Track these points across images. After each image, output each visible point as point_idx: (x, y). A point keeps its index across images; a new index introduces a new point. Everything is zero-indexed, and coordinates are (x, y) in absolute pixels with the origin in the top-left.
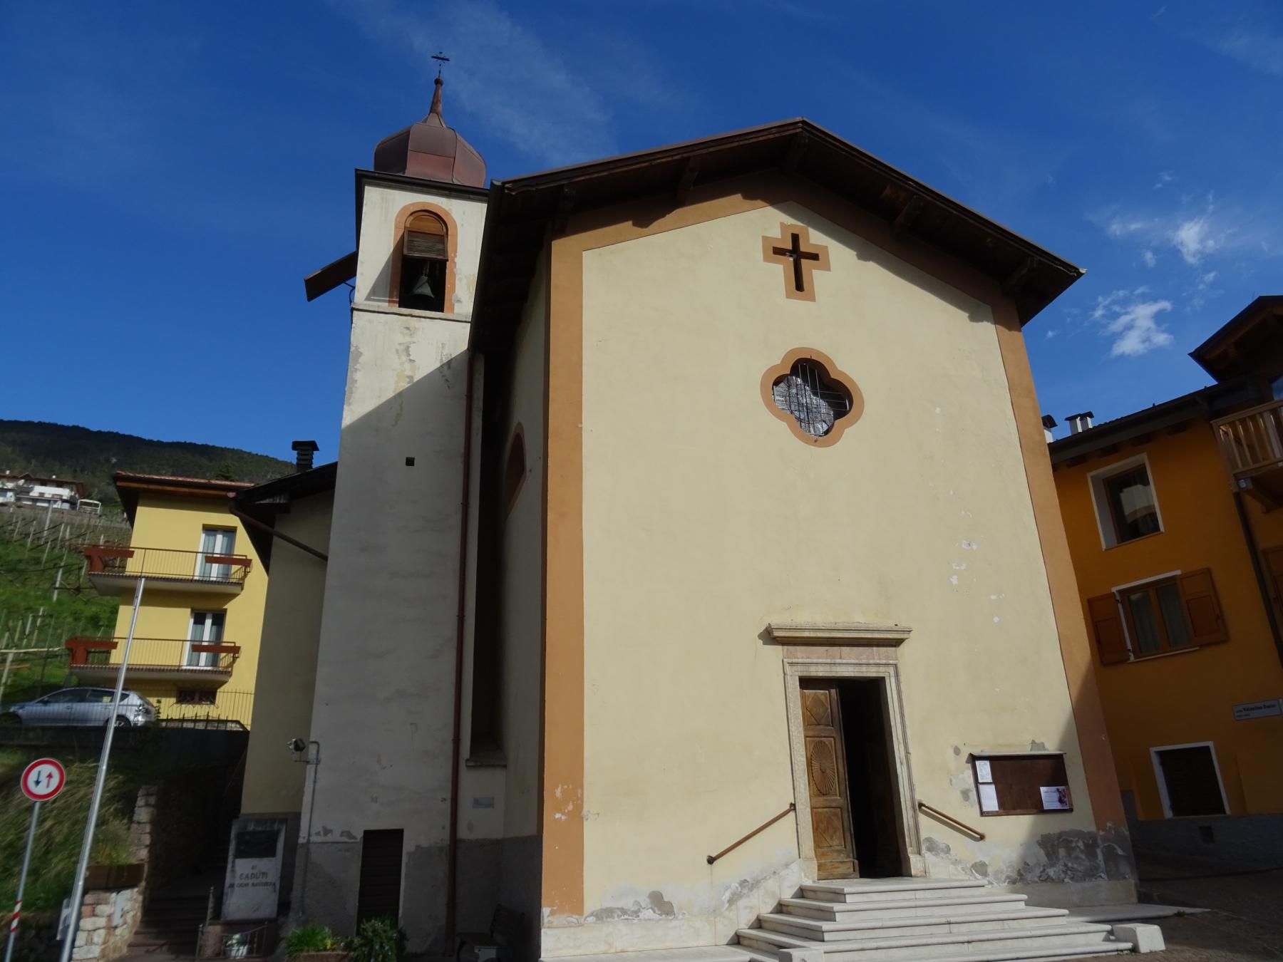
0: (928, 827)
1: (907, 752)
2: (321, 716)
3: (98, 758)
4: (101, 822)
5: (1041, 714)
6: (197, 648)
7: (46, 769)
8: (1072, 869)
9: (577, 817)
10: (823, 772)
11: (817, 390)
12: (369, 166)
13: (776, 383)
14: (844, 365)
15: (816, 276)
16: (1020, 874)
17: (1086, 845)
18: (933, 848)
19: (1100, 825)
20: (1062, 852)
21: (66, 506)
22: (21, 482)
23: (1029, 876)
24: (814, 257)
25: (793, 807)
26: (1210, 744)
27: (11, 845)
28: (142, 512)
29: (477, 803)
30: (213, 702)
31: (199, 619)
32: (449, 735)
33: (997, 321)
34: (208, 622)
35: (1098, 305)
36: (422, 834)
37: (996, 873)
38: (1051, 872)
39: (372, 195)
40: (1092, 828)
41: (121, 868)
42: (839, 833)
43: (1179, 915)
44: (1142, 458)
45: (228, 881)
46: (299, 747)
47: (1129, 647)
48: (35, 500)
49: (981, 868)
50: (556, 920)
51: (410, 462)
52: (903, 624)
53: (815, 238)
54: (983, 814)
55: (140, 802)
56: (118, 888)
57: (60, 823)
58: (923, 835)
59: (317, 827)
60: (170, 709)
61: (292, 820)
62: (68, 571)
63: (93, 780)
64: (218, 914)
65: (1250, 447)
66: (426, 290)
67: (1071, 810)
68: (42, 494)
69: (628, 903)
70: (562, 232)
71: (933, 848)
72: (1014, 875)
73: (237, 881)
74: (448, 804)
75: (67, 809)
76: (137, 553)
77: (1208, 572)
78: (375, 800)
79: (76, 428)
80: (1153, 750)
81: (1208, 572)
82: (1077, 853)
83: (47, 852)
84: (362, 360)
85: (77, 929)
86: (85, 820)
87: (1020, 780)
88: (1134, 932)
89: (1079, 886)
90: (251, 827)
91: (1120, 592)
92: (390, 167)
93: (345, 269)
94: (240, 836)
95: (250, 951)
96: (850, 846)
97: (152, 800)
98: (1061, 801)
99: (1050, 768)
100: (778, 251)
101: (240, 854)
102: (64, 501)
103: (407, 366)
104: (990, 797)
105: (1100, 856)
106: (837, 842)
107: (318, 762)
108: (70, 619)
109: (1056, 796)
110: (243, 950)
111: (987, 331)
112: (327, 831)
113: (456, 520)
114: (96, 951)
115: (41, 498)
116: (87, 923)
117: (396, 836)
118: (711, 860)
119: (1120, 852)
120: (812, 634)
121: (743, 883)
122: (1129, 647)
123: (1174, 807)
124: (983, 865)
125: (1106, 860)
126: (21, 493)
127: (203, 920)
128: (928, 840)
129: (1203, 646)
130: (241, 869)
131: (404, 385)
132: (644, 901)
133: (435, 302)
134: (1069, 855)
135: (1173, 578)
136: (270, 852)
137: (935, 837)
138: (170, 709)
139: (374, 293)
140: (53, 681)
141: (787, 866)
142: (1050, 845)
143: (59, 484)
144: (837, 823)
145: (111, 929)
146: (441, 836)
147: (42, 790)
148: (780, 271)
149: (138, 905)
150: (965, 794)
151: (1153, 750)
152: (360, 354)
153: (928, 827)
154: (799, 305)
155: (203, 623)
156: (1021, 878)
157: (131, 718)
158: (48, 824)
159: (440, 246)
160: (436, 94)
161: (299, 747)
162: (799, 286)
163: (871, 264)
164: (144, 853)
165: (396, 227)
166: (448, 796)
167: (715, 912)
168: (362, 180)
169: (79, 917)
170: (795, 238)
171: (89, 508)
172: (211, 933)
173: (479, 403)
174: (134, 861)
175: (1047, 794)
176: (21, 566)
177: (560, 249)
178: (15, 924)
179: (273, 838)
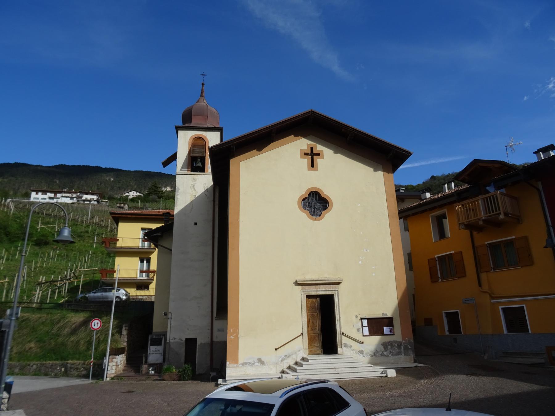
0: (345, 340)
1: (340, 317)
2: (172, 305)
3: (111, 316)
4: (113, 335)
5: (387, 304)
6: (142, 272)
7: (96, 321)
8: (392, 352)
9: (237, 337)
10: (313, 323)
11: (316, 203)
12: (181, 124)
13: (304, 200)
14: (327, 192)
15: (319, 161)
16: (374, 354)
17: (398, 345)
18: (346, 346)
19: (403, 339)
20: (389, 347)
21: (96, 203)
22: (79, 194)
23: (377, 354)
24: (318, 155)
25: (302, 334)
26: (458, 311)
27: (89, 341)
28: (120, 224)
29: (219, 330)
30: (148, 289)
31: (142, 261)
32: (210, 309)
33: (384, 170)
34: (145, 262)
35: (551, 82)
36: (202, 339)
37: (366, 354)
38: (385, 353)
39: (181, 133)
40: (401, 340)
41: (119, 349)
42: (318, 341)
43: (416, 366)
44: (445, 210)
45: (149, 352)
46: (166, 314)
47: (440, 276)
48: (84, 201)
49: (361, 352)
50: (231, 365)
51: (196, 224)
52: (341, 278)
53: (319, 148)
54: (363, 336)
55: (124, 329)
56: (118, 354)
57: (102, 334)
58: (343, 342)
59: (172, 337)
60: (133, 292)
61: (165, 334)
62: (98, 235)
63: (110, 322)
64: (146, 362)
65: (473, 210)
66: (200, 165)
67: (394, 334)
68: (86, 198)
69: (251, 361)
70: (234, 156)
71: (346, 346)
72: (372, 354)
73: (151, 352)
74: (210, 330)
75: (104, 330)
76: (120, 240)
77: (461, 252)
78: (188, 329)
79: (97, 167)
80: (444, 312)
81: (461, 252)
82: (395, 347)
83: (99, 343)
84: (180, 191)
85: (108, 365)
86: (108, 334)
87: (376, 325)
88: (387, 371)
89: (394, 357)
90: (154, 337)
91: (438, 257)
92: (187, 121)
93: (174, 157)
94: (151, 340)
95: (155, 372)
96: (321, 345)
97: (127, 328)
98: (390, 332)
99: (389, 321)
100: (306, 154)
101: (152, 345)
102: (95, 201)
103: (194, 192)
104: (366, 331)
105: (402, 348)
106: (317, 344)
107: (171, 318)
108: (100, 254)
109: (389, 330)
110: (153, 372)
111: (380, 174)
112: (175, 339)
113: (211, 242)
114: (114, 372)
115: (86, 200)
116: (111, 364)
117: (195, 340)
118: (276, 349)
119: (409, 347)
120: (310, 282)
121: (286, 356)
122: (440, 276)
123: (449, 331)
124: (362, 351)
125: (404, 350)
126: (79, 198)
127: (142, 363)
128: (345, 343)
129: (459, 278)
130: (152, 349)
131: (193, 198)
132: (256, 360)
133: (202, 169)
134: (392, 348)
135: (451, 254)
136: (160, 344)
137: (347, 343)
138: (133, 292)
139: (183, 168)
140: (96, 279)
141: (299, 351)
142: (385, 345)
143: (93, 194)
144: (317, 338)
145: (117, 365)
146: (208, 340)
147: (96, 327)
148: (306, 161)
149: (125, 359)
150: (358, 330)
151: (444, 312)
152: (179, 189)
153: (345, 340)
154: (313, 172)
155: (143, 262)
156: (375, 354)
157: (122, 297)
158: (98, 335)
159: (203, 151)
160: (202, 90)
161: (166, 314)
162: (313, 166)
163: (339, 155)
164: (125, 344)
165: (189, 144)
166: (210, 328)
167: (277, 364)
168: (178, 128)
169: (108, 362)
170: (312, 149)
171: (104, 203)
172: (144, 367)
173: (217, 202)
174: (123, 346)
175: (386, 330)
176: (82, 234)
177: (233, 161)
178: (92, 364)
179: (161, 340)
